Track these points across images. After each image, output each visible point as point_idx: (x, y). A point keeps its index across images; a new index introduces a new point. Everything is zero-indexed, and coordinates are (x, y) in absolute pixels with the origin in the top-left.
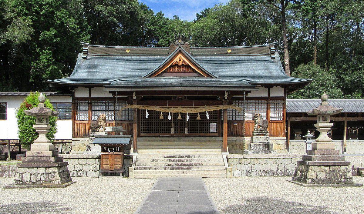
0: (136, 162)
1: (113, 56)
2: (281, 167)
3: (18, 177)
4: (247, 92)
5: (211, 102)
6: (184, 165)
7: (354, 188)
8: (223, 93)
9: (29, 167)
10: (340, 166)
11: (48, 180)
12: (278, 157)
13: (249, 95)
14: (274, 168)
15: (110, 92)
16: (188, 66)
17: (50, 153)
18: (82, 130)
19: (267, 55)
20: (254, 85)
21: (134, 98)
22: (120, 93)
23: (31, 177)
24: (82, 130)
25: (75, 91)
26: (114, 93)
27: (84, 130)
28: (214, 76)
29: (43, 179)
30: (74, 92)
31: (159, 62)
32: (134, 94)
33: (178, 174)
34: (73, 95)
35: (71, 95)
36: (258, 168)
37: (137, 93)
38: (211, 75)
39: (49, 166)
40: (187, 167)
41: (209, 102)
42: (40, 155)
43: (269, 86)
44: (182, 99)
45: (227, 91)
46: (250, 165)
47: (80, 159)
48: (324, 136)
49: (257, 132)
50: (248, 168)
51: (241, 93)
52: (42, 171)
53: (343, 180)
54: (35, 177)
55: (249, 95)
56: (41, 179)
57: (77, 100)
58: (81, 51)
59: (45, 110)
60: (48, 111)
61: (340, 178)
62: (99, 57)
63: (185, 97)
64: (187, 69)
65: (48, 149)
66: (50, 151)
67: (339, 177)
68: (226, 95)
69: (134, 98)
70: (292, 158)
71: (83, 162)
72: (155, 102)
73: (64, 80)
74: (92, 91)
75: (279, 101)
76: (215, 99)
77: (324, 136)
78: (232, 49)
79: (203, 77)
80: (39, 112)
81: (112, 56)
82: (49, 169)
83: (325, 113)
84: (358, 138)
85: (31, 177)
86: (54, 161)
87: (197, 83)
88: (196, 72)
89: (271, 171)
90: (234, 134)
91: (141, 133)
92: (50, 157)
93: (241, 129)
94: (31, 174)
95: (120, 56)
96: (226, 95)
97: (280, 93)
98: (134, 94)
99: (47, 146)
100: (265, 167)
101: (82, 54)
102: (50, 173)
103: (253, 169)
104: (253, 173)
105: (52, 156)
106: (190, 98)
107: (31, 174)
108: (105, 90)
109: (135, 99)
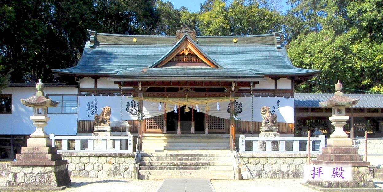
0: (141, 161)
1: (120, 45)
2: (292, 168)
3: (10, 177)
4: (256, 83)
5: (218, 94)
6: (190, 165)
7: (307, 187)
8: (230, 84)
9: (23, 166)
10: (360, 167)
11: (43, 182)
12: (289, 156)
13: (257, 87)
14: (285, 169)
15: (116, 83)
16: (194, 55)
17: (47, 150)
18: (87, 126)
19: (272, 45)
20: (262, 76)
21: (140, 89)
22: (126, 84)
23: (25, 178)
24: (87, 126)
25: (80, 82)
26: (119, 83)
27: (89, 126)
28: (220, 66)
29: (38, 179)
30: (80, 83)
31: (164, 51)
32: (140, 85)
33: (184, 175)
34: (79, 87)
35: (76, 86)
36: (267, 168)
37: (143, 84)
38: (217, 65)
39: (45, 164)
40: (193, 166)
41: (216, 94)
42: (36, 151)
43: (276, 78)
44: (188, 90)
45: (234, 82)
46: (259, 165)
47: (82, 157)
48: (339, 132)
49: (265, 127)
50: (257, 169)
51: (248, 84)
52: (37, 170)
53: (363, 184)
54: (29, 178)
55: (257, 87)
56: (35, 181)
57: (82, 92)
58: (89, 40)
59: (43, 100)
60: (46, 100)
61: (359, 181)
62: (106, 45)
63: (191, 89)
64: (193, 59)
65: (45, 145)
66: (47, 146)
67: (358, 180)
68: (233, 86)
69: (140, 89)
70: (303, 158)
71: (85, 160)
72: (161, 94)
73: (68, 71)
74: (98, 81)
75: (287, 94)
76: (222, 90)
77: (339, 132)
78: (238, 38)
79: (210, 68)
80: (36, 101)
81: (119, 45)
82: (45, 168)
83: (340, 104)
84: (357, 136)
85: (25, 178)
86: (51, 159)
87: (204, 73)
88: (202, 62)
89: (282, 172)
90: (242, 130)
91: (147, 128)
92: (46, 154)
93: (249, 125)
94: (25, 174)
95: (127, 45)
96: (233, 86)
97: (285, 85)
98: (140, 85)
99: (43, 142)
100: (275, 167)
101: (89, 42)
102: (46, 173)
103: (262, 169)
104: (263, 175)
105: (49, 153)
106: (197, 90)
107: (25, 174)
108: (110, 80)
109: (140, 91)
